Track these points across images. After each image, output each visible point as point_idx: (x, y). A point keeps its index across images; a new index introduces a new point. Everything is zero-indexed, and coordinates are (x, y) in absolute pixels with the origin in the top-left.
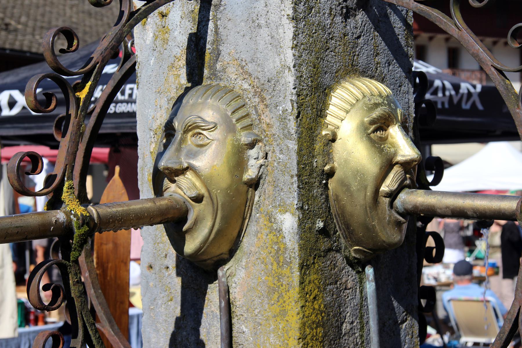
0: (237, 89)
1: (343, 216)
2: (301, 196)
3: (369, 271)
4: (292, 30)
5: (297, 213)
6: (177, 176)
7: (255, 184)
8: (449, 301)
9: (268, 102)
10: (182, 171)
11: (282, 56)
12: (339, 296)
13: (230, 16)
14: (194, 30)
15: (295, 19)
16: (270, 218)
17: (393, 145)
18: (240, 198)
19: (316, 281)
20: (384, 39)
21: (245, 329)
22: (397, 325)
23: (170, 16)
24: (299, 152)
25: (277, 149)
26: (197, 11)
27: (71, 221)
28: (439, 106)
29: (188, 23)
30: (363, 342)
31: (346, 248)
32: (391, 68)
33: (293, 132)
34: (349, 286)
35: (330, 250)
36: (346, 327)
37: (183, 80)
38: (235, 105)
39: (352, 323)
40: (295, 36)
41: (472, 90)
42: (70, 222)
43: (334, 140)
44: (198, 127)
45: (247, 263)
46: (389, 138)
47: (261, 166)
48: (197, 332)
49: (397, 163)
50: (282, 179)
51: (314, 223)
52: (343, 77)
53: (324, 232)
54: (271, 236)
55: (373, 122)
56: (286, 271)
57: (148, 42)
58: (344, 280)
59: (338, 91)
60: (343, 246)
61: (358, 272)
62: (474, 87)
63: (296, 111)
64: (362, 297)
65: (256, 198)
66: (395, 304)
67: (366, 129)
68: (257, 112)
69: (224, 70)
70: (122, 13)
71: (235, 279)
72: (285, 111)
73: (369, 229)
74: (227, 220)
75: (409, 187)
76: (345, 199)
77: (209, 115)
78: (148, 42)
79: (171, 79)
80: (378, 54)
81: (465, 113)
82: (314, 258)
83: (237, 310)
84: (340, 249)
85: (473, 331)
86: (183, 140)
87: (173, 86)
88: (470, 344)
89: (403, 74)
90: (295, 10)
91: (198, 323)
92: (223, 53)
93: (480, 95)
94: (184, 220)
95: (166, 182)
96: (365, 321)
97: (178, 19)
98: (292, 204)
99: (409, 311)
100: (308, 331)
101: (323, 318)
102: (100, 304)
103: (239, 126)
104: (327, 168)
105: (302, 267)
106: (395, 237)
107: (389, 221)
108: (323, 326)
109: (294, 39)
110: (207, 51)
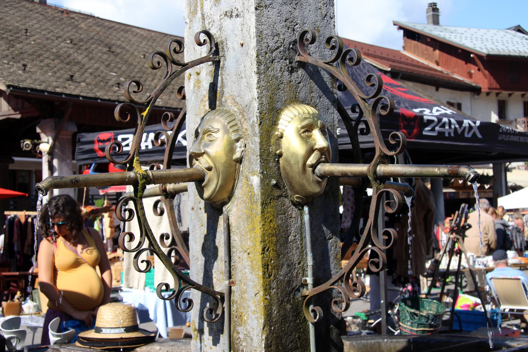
0: (232, 111)
1: (288, 179)
2: (262, 167)
3: (306, 209)
4: (257, 79)
5: (260, 175)
6: (199, 157)
7: (240, 161)
8: (491, 279)
9: (246, 117)
10: (201, 154)
11: (252, 93)
12: (286, 221)
13: (228, 73)
14: (212, 81)
15: (258, 73)
16: (247, 179)
17: (314, 140)
18: (233, 167)
19: (272, 212)
20: (316, 84)
21: (236, 239)
22: (325, 241)
23: (201, 74)
24: (261, 143)
25: (250, 142)
26: (213, 71)
27: (137, 177)
28: (447, 135)
29: (209, 78)
30: (302, 247)
31: (291, 196)
32: (321, 99)
33: (257, 132)
34: (293, 216)
35: (281, 196)
36: (291, 238)
37: (207, 108)
38: (229, 119)
39: (295, 236)
40: (259, 82)
41: (473, 124)
42: (137, 177)
43: (282, 137)
44: (210, 131)
45: (237, 203)
46: (313, 136)
47: (242, 151)
48: (214, 241)
49: (316, 149)
50: (252, 158)
51: (270, 181)
52: (289, 104)
53: (276, 186)
54: (248, 188)
55: (302, 128)
56: (255, 206)
57: (191, 88)
58: (290, 213)
59: (285, 111)
60: (289, 195)
61: (299, 209)
62: (475, 123)
63: (259, 122)
64: (302, 223)
65: (241, 169)
66: (325, 228)
67: (299, 131)
68: (241, 123)
69: (226, 101)
70: (168, 72)
71: (232, 212)
72: (253, 122)
73: (302, 186)
74: (226, 181)
75: (324, 162)
76: (288, 169)
77: (217, 125)
78: (191, 88)
79: (202, 107)
80: (312, 92)
81: (450, 138)
82: (271, 200)
83: (233, 229)
84: (288, 196)
85: (508, 301)
86: (202, 138)
87: (203, 111)
88: (507, 311)
89: (330, 103)
90: (258, 69)
91: (215, 237)
92: (225, 92)
93: (479, 128)
94: (204, 181)
95: (194, 160)
96: (304, 236)
97: (205, 75)
98: (257, 171)
99: (334, 233)
100: (266, 238)
101: (276, 232)
102: (177, 235)
103: (231, 130)
104: (278, 152)
105: (262, 204)
106: (316, 189)
107: (313, 181)
108: (276, 236)
109: (258, 83)
110: (218, 92)
